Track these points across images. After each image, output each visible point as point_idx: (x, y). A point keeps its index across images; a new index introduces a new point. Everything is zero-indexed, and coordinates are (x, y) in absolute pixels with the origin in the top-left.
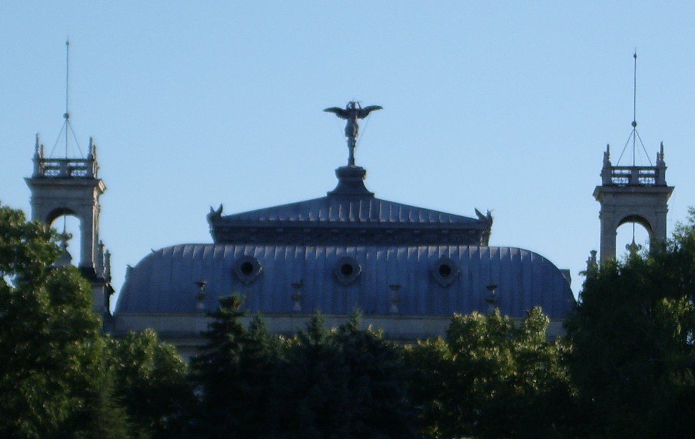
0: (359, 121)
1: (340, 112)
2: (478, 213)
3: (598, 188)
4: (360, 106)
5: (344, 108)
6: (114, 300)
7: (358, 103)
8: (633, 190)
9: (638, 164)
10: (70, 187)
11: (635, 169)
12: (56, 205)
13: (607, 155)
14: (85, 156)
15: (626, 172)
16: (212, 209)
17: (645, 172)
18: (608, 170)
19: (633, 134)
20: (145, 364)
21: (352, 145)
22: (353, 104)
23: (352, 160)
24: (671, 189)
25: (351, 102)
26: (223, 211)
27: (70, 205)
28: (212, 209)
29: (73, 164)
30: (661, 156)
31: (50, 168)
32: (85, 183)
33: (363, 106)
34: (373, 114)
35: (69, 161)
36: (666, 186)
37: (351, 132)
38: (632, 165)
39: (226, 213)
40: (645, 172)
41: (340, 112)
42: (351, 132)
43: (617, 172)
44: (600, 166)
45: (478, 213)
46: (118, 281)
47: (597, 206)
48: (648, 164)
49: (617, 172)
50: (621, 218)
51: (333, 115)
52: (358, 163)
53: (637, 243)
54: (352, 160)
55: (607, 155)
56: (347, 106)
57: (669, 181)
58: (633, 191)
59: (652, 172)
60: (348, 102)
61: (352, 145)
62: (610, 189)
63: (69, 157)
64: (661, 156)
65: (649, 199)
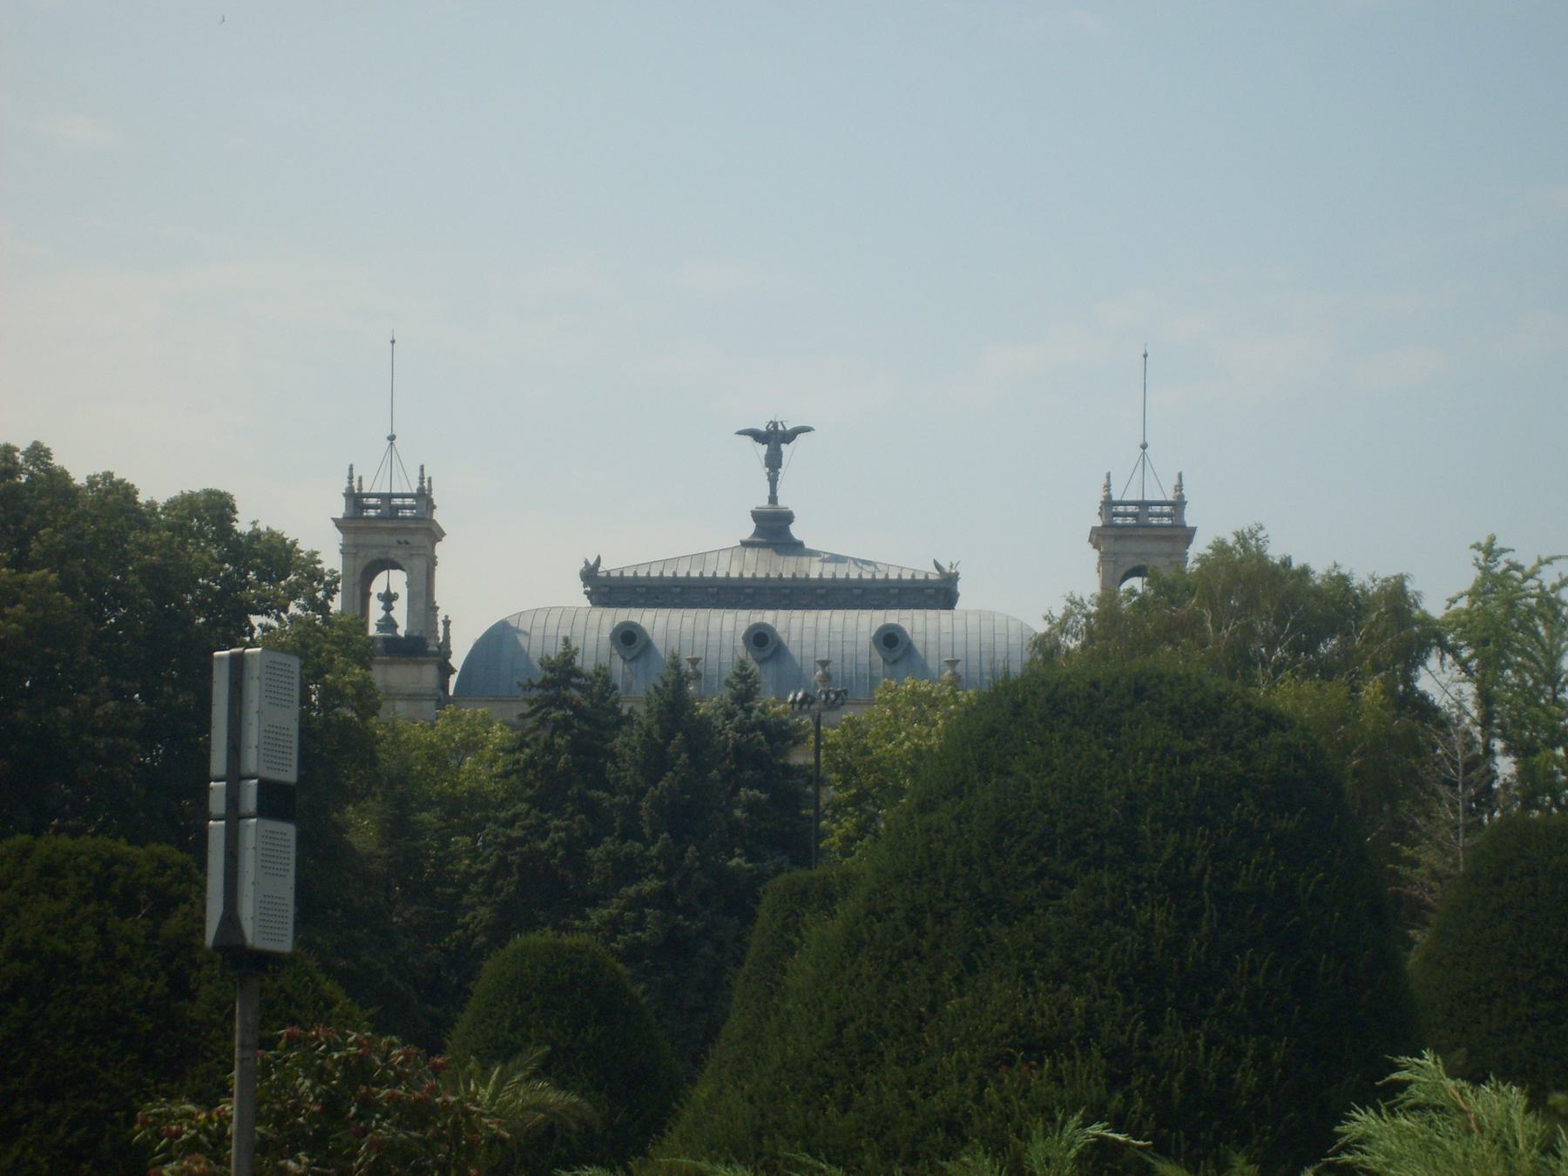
0: (784, 447)
1: (757, 436)
2: (938, 566)
3: (1094, 530)
4: (784, 427)
5: (763, 429)
6: (453, 680)
7: (782, 423)
8: (1141, 532)
9: (1148, 498)
10: (393, 531)
11: (1143, 504)
12: (375, 554)
13: (1108, 487)
14: (414, 488)
15: (1131, 509)
16: (587, 563)
17: (1157, 509)
18: (1108, 504)
19: (1141, 462)
20: (92, 905)
21: (773, 481)
22: (775, 425)
23: (773, 499)
24: (1193, 530)
25: (771, 422)
26: (601, 564)
27: (395, 554)
28: (587, 563)
29: (397, 501)
30: (1179, 487)
31: (404, 507)
32: (413, 526)
33: (789, 428)
34: (800, 437)
35: (392, 496)
36: (1184, 526)
37: (774, 463)
38: (1140, 499)
39: (605, 567)
40: (1157, 509)
41: (757, 436)
42: (774, 463)
43: (1121, 509)
44: (1099, 497)
45: (938, 566)
46: (457, 660)
47: (1094, 555)
48: (1160, 498)
49: (1121, 509)
50: (1122, 572)
51: (749, 440)
52: (783, 502)
53: (393, 591)
54: (773, 499)
55: (1108, 487)
56: (767, 427)
57: (1189, 520)
58: (1140, 533)
59: (1167, 509)
60: (769, 421)
61: (773, 481)
62: (1110, 532)
63: (394, 491)
64: (1179, 487)
65: (1167, 547)
